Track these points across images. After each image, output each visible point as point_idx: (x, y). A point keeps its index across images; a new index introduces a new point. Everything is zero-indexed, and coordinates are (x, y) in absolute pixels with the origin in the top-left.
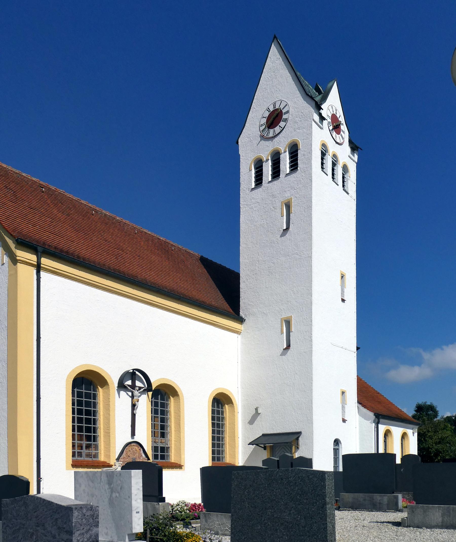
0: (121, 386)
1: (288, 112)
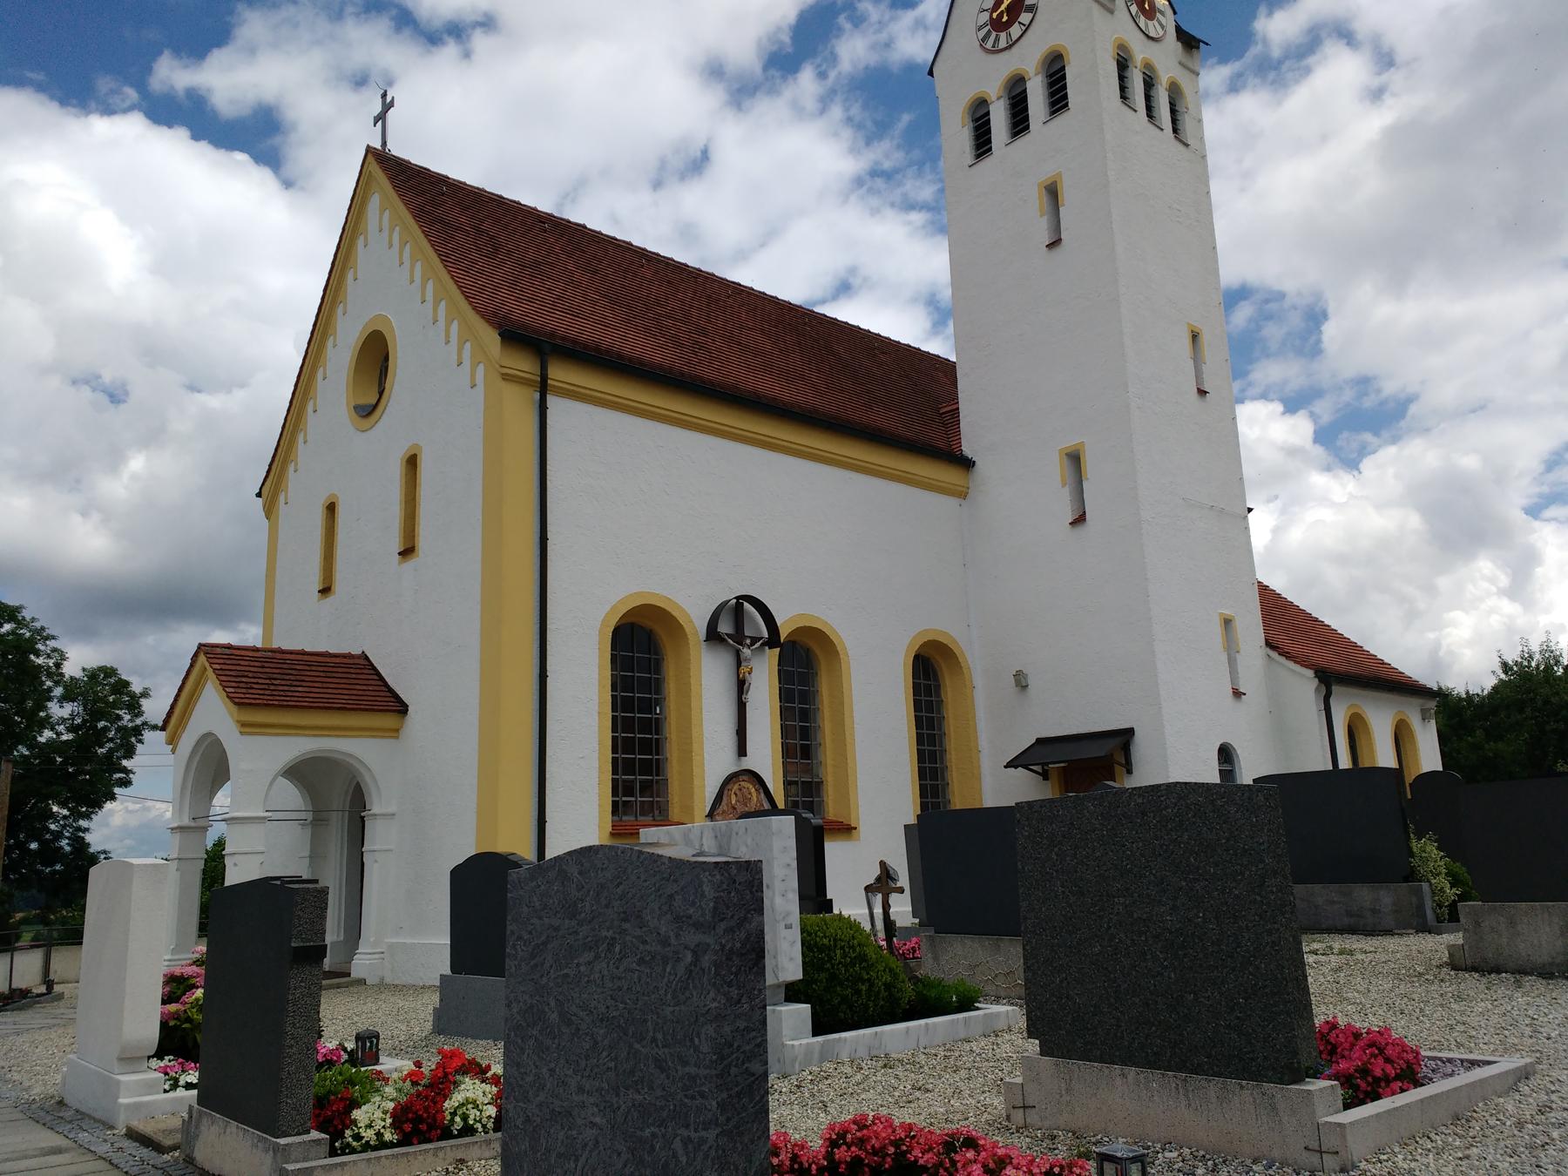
0: (713, 636)
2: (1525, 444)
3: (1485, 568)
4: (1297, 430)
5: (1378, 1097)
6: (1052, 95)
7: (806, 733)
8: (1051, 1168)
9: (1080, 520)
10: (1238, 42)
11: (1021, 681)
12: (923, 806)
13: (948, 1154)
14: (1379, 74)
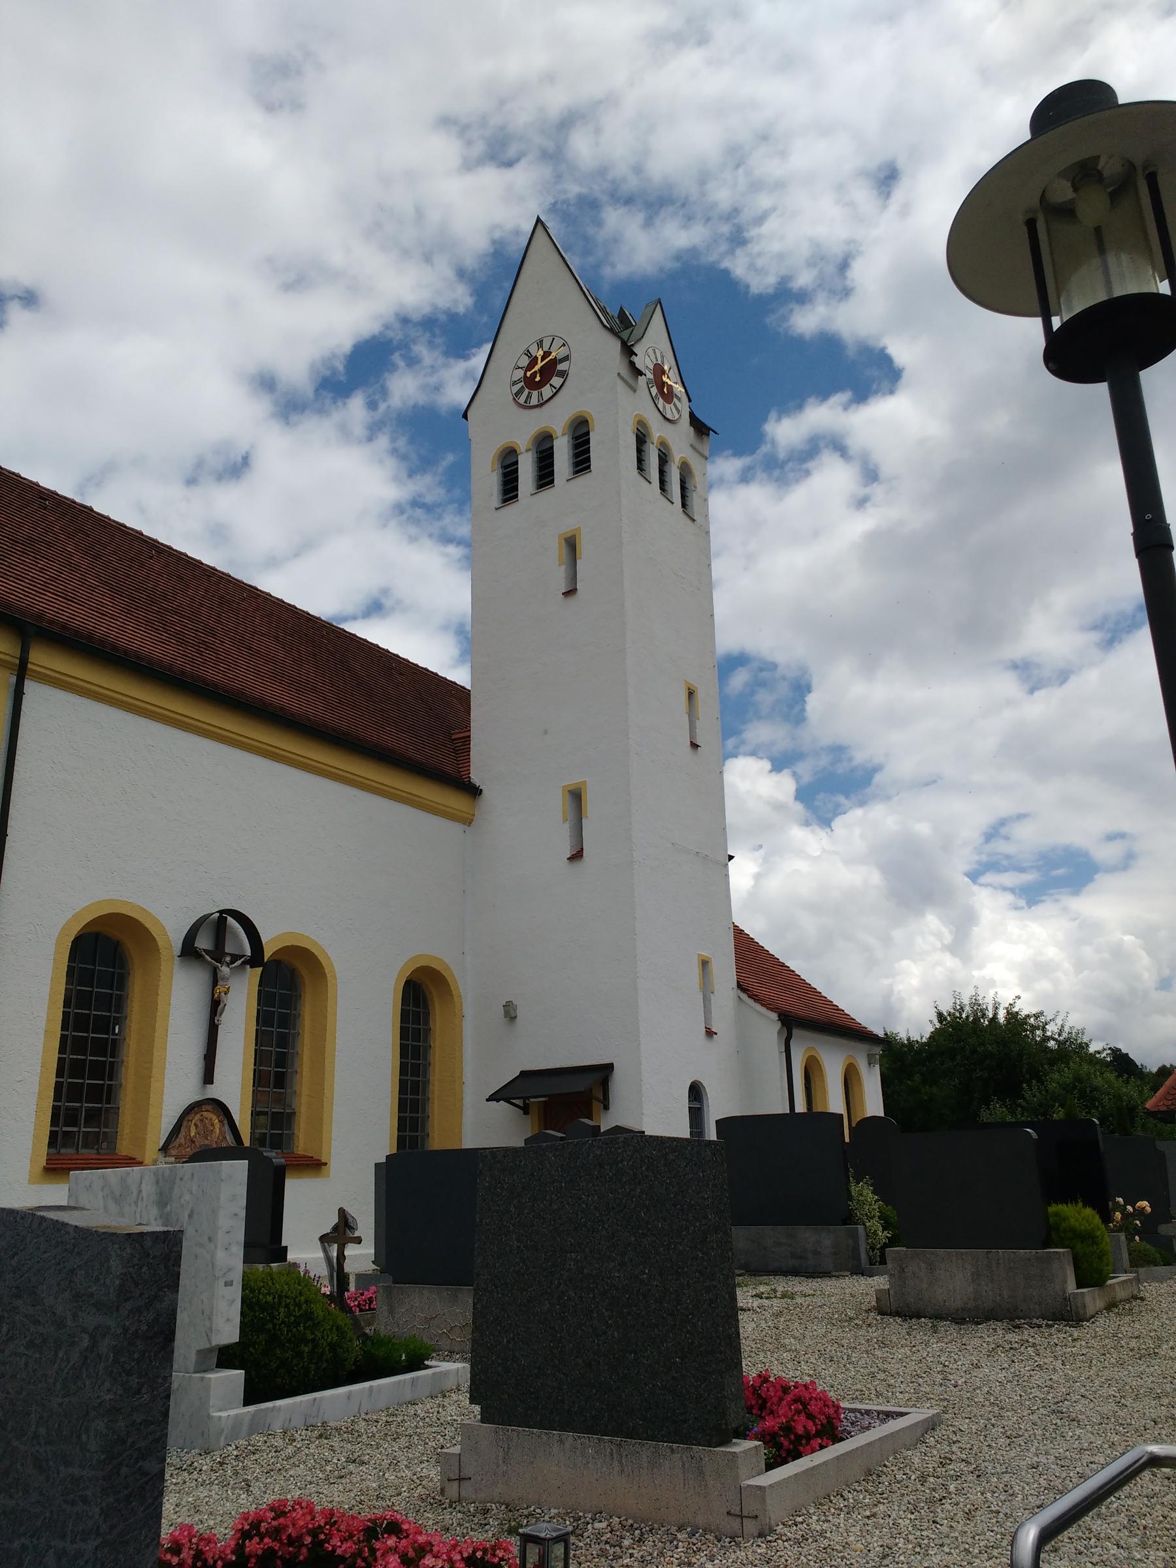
0: (189, 951)
1: (566, 358)
2: (969, 816)
3: (933, 924)
4: (782, 787)
5: (798, 1456)
6: (576, 455)
7: (283, 1060)
8: (474, 1552)
9: (577, 855)
10: (748, 440)
11: (510, 1013)
12: (401, 1142)
13: (368, 1541)
14: (865, 486)
